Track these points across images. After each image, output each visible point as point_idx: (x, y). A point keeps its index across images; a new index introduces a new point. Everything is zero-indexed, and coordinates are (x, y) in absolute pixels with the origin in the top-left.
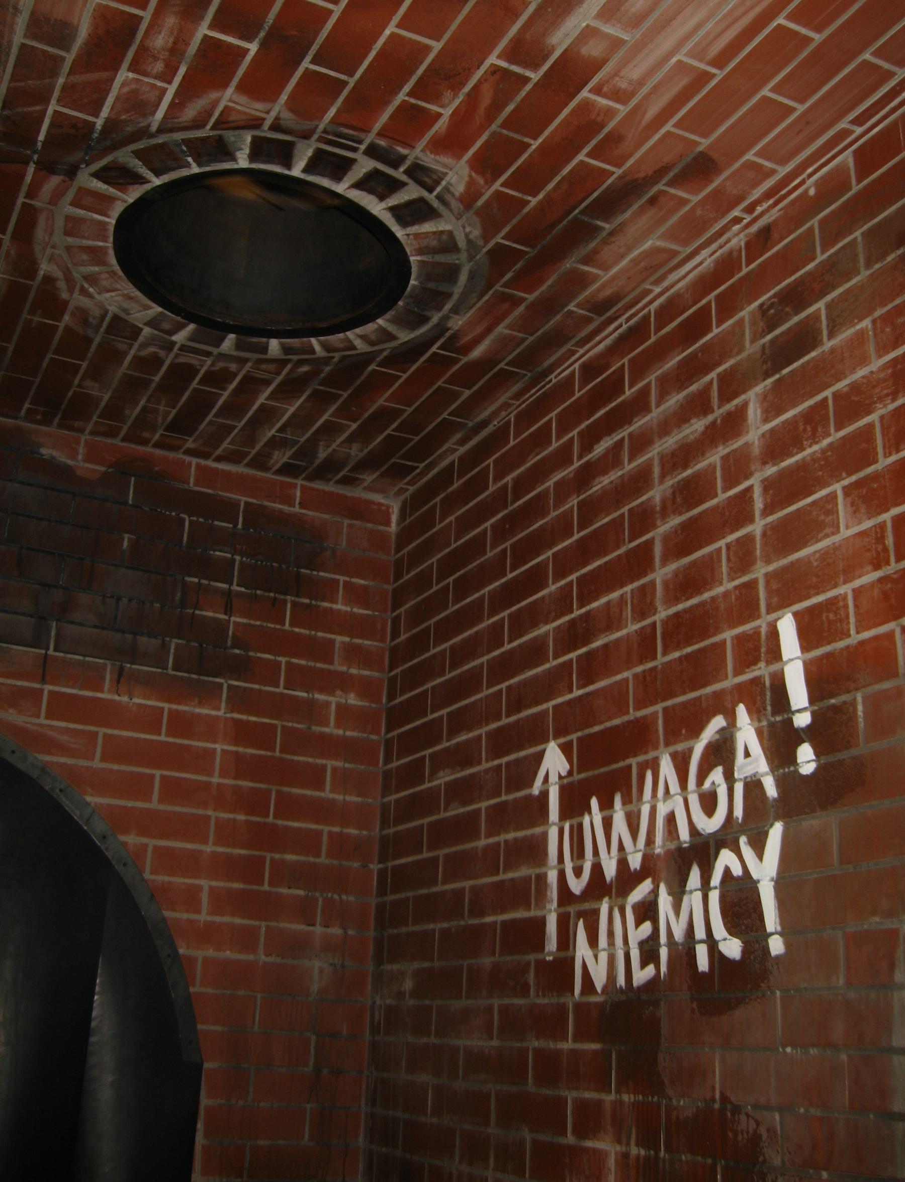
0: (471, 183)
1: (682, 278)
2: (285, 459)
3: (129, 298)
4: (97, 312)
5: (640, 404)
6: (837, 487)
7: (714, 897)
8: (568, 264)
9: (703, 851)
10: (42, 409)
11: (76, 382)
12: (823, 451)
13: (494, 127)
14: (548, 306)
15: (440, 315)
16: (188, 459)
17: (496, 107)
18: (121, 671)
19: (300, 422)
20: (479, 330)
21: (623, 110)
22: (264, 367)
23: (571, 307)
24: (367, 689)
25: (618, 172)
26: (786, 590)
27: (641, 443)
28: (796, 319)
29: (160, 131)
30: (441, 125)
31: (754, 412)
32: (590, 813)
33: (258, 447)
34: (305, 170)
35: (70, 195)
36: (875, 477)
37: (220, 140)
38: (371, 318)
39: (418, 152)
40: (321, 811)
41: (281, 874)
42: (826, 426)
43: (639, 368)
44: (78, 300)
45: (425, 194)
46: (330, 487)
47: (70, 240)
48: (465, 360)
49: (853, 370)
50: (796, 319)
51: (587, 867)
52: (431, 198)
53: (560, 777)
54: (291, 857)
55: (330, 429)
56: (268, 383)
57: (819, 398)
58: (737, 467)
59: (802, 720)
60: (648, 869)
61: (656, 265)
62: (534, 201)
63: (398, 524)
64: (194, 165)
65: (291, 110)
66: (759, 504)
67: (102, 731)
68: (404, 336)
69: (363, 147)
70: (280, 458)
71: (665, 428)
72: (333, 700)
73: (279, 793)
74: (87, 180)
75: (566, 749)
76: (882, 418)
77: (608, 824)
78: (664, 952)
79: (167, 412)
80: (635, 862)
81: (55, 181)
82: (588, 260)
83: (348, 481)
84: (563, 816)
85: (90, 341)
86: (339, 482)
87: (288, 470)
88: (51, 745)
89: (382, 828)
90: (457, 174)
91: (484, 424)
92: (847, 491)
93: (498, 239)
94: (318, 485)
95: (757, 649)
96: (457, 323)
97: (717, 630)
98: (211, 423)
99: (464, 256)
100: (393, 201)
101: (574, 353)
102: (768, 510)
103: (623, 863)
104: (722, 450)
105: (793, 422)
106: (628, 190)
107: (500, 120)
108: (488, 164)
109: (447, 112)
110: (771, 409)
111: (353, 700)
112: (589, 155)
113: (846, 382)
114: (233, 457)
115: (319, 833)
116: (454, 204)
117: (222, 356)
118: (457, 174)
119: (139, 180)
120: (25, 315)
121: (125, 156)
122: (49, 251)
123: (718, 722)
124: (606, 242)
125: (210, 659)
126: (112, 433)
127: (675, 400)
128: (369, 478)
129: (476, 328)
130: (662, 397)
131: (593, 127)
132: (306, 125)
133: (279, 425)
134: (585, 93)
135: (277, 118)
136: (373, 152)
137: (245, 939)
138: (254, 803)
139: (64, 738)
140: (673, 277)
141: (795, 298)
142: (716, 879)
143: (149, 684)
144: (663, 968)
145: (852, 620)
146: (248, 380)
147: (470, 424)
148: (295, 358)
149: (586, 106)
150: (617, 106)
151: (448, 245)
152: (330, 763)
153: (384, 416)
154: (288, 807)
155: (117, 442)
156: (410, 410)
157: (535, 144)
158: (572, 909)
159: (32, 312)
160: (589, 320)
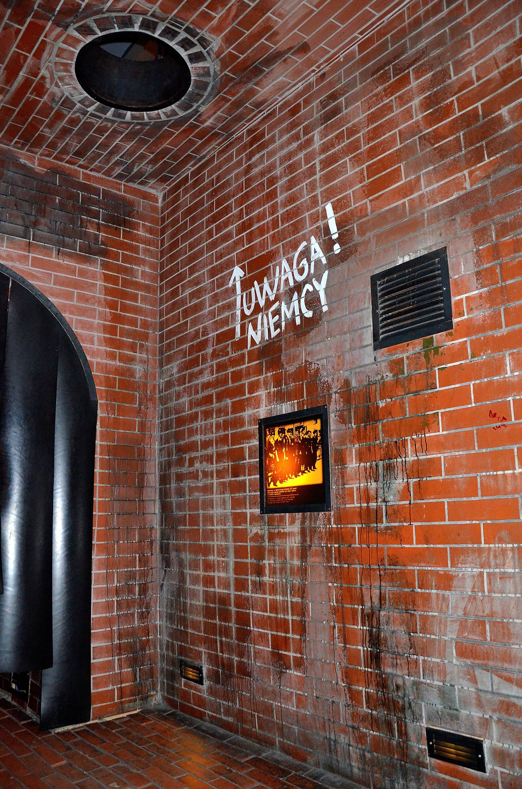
0: (221, 47)
1: (289, 94)
2: (119, 171)
3: (75, 88)
4: (59, 94)
5: (272, 140)
6: (347, 159)
7: (303, 301)
8: (250, 85)
9: (298, 287)
10: (22, 141)
11: (41, 129)
12: (342, 148)
13: (234, 24)
14: (238, 104)
15: (197, 105)
16: (79, 169)
17: (236, 16)
18: (59, 250)
19: (130, 153)
20: (211, 112)
21: (281, 22)
22: (122, 125)
23: (247, 105)
24: (152, 266)
25: (275, 47)
26: (328, 196)
27: (271, 154)
28: (334, 104)
29: (108, 11)
30: (215, 22)
31: (316, 138)
32: (254, 287)
33: (110, 165)
34: (160, 35)
35: (64, 36)
36: (361, 153)
37: (130, 18)
38: (170, 104)
39: (204, 33)
40: (137, 310)
41: (123, 333)
42: (343, 139)
43: (271, 128)
44: (54, 89)
45: (203, 50)
46: (135, 186)
47: (57, 59)
48: (202, 126)
49: (354, 119)
50: (334, 104)
51: (253, 305)
52: (204, 52)
53: (241, 278)
54: (127, 327)
55: (142, 157)
56: (122, 133)
57: (341, 130)
58: (309, 158)
59: (335, 237)
60: (277, 298)
61: (281, 88)
62: (242, 57)
63: (162, 203)
64: (117, 28)
65: (161, 9)
66: (318, 168)
67: (54, 273)
68: (181, 114)
69: (184, 27)
70: (118, 170)
71: (282, 147)
72: (140, 269)
73: (121, 302)
74: (72, 32)
75: (243, 268)
76: (363, 134)
77: (261, 289)
78: (283, 324)
79: (76, 146)
80: (272, 298)
81: (59, 30)
82: (257, 84)
83: (142, 183)
84: (243, 291)
85: (53, 109)
86: (139, 184)
87: (120, 177)
88: (34, 277)
89: (160, 318)
90: (216, 42)
91: (204, 156)
92: (350, 160)
93: (226, 72)
94: (130, 184)
95: (318, 217)
96: (202, 109)
97: (303, 213)
98: (94, 152)
99: (211, 79)
100: (190, 52)
101: (244, 125)
102: (322, 170)
103: (267, 300)
104: (304, 152)
105: (332, 139)
106: (278, 55)
107: (237, 22)
108: (228, 40)
109: (218, 16)
110: (324, 135)
111: (147, 270)
112: (266, 40)
113: (351, 123)
114: (97, 170)
115: (137, 319)
116: (213, 55)
117: (106, 119)
118: (216, 42)
119: (93, 33)
120: (28, 95)
121: (90, 22)
122: (47, 64)
123: (304, 244)
124: (265, 77)
125: (91, 251)
126: (49, 155)
127: (285, 137)
128: (152, 182)
129: (209, 113)
130: (280, 137)
131: (269, 28)
132: (165, 15)
133: (121, 154)
134: (269, 14)
135: (154, 11)
136: (188, 30)
137: (112, 356)
138: (112, 306)
139: (39, 275)
140: (287, 94)
141: (333, 97)
142: (303, 294)
143: (70, 256)
144: (283, 328)
145: (352, 201)
146: (114, 131)
147: (198, 157)
148: (135, 121)
149: (269, 18)
150: (279, 20)
151: (206, 72)
152: (140, 293)
153: (166, 151)
154: (125, 308)
155: (50, 159)
156: (176, 149)
157: (248, 33)
158: (246, 321)
159: (31, 93)
160: (253, 110)
